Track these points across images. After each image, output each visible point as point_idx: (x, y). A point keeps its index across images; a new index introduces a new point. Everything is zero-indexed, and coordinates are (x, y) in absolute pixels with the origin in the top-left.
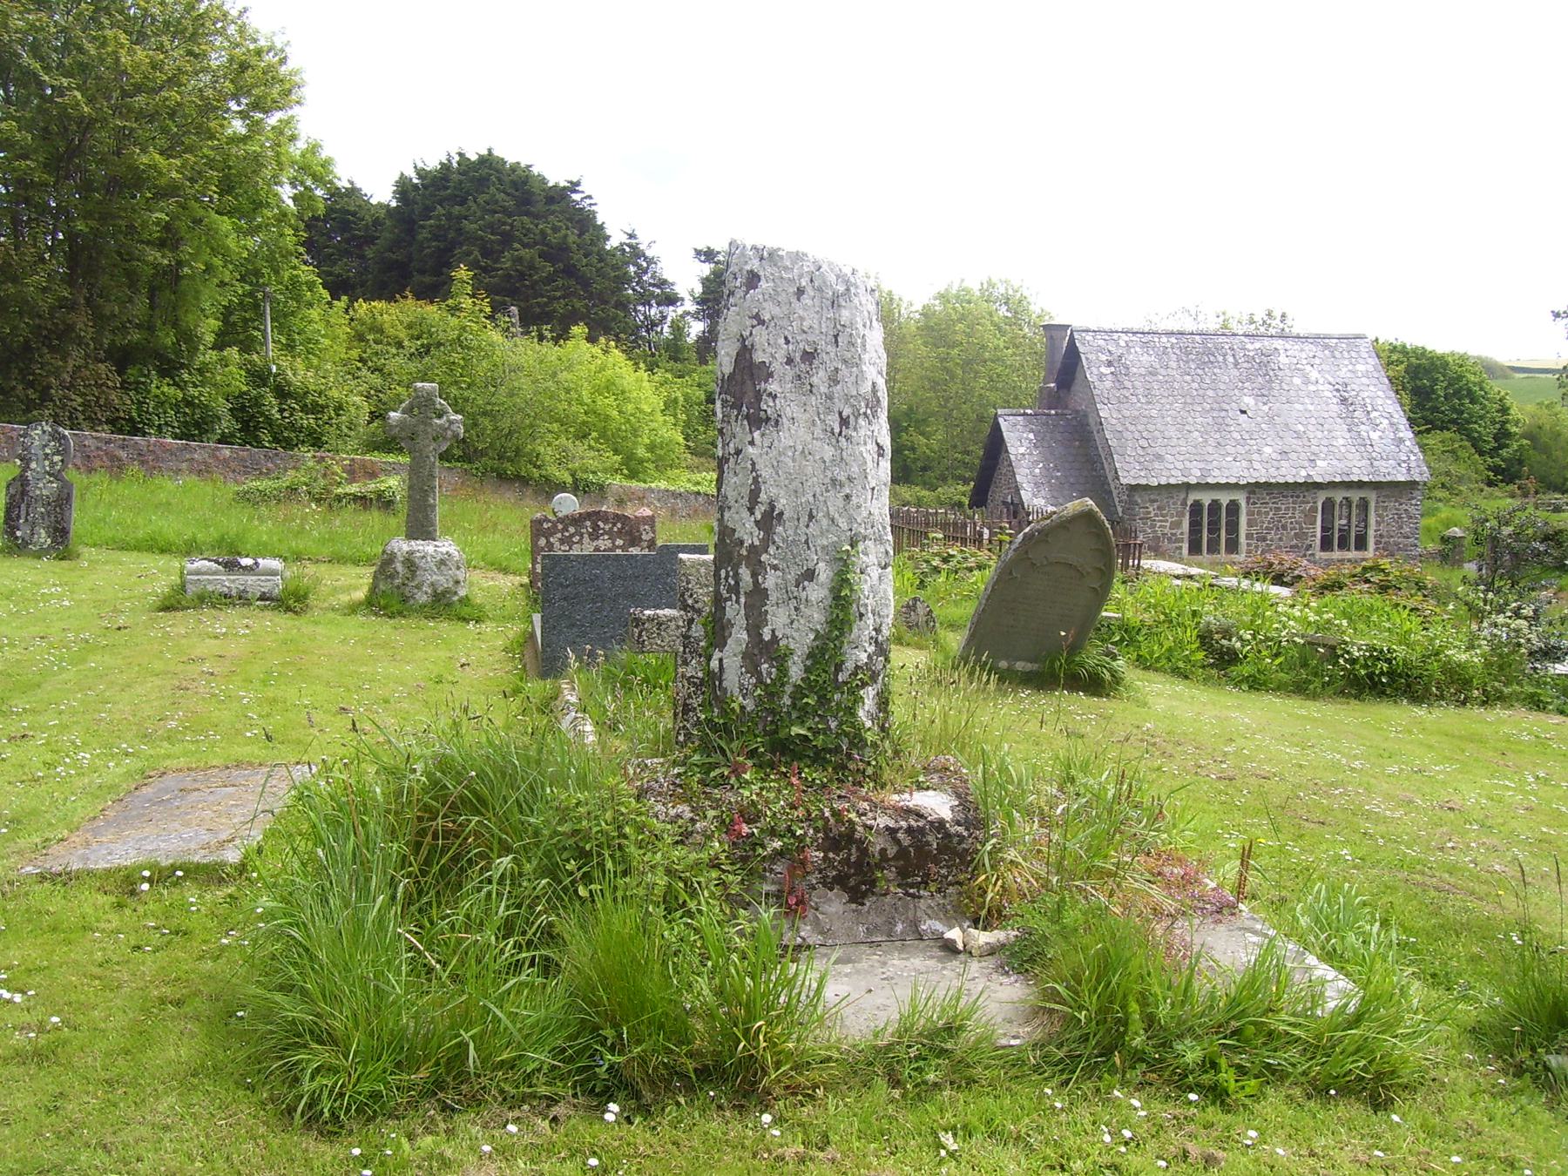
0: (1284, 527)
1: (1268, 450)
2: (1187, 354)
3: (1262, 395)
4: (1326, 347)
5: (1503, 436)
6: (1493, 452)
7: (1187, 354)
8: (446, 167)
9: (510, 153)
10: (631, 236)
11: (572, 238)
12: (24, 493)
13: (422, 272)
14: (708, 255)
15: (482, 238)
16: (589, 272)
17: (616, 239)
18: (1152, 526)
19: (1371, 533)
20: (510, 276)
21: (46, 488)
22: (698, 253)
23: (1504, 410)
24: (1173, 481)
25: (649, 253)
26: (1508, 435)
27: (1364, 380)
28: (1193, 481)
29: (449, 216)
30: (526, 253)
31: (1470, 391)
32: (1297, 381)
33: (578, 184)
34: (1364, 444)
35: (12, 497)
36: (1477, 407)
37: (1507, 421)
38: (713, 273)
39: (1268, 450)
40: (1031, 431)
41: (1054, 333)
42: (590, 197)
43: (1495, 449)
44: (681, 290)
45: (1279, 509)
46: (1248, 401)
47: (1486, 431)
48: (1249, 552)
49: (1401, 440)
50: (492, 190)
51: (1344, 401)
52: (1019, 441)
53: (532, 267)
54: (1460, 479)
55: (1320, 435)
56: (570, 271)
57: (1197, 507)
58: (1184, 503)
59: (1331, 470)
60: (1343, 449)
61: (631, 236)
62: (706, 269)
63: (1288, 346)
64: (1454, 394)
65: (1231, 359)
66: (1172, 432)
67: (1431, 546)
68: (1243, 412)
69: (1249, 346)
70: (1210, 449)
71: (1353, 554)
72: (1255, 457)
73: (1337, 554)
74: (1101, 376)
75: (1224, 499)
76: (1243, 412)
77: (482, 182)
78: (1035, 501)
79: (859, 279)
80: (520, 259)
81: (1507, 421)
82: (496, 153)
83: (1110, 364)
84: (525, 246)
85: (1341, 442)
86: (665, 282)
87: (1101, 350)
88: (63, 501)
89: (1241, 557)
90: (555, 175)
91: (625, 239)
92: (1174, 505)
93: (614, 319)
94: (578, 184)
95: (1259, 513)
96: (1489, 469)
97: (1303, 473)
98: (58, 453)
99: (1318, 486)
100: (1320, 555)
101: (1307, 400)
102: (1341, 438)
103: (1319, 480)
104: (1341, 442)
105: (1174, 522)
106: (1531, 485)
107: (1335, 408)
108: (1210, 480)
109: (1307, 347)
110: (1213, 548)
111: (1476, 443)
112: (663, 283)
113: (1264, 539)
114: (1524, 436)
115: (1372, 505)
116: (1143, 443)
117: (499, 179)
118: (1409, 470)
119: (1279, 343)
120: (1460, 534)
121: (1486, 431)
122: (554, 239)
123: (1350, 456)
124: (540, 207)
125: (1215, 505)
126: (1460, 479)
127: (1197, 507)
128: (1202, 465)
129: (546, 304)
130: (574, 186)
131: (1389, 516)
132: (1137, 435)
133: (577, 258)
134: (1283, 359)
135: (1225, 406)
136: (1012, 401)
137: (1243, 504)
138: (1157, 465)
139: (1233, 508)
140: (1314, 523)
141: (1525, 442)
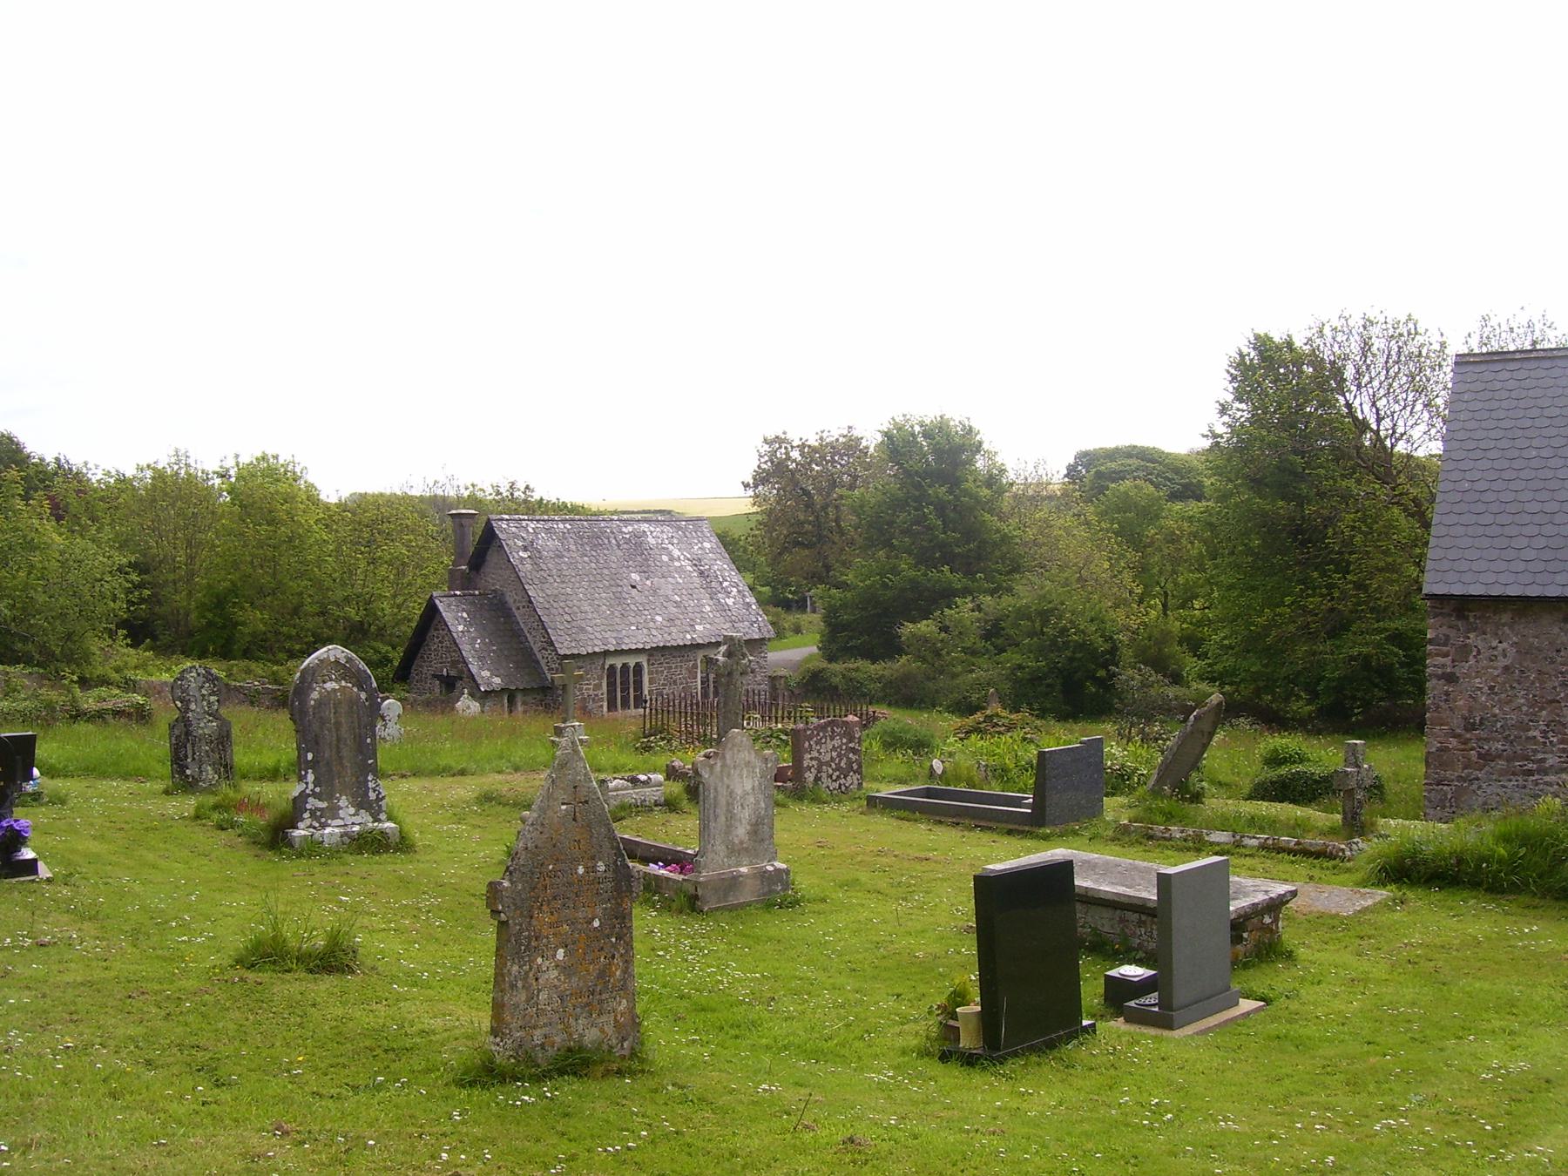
1: (659, 618)
3: (645, 572)
4: (679, 528)
12: (188, 733)
21: (207, 727)
24: (597, 650)
28: (612, 649)
32: (665, 558)
34: (724, 609)
35: (177, 737)
39: (659, 618)
41: (464, 521)
49: (749, 605)
52: (456, 618)
57: (612, 667)
83: (525, 549)
87: (516, 536)
88: (223, 740)
98: (213, 693)
99: (699, 646)
105: (595, 686)
108: (624, 647)
116: (567, 617)
127: (612, 667)
134: (651, 540)
137: (645, 665)
138: (582, 636)
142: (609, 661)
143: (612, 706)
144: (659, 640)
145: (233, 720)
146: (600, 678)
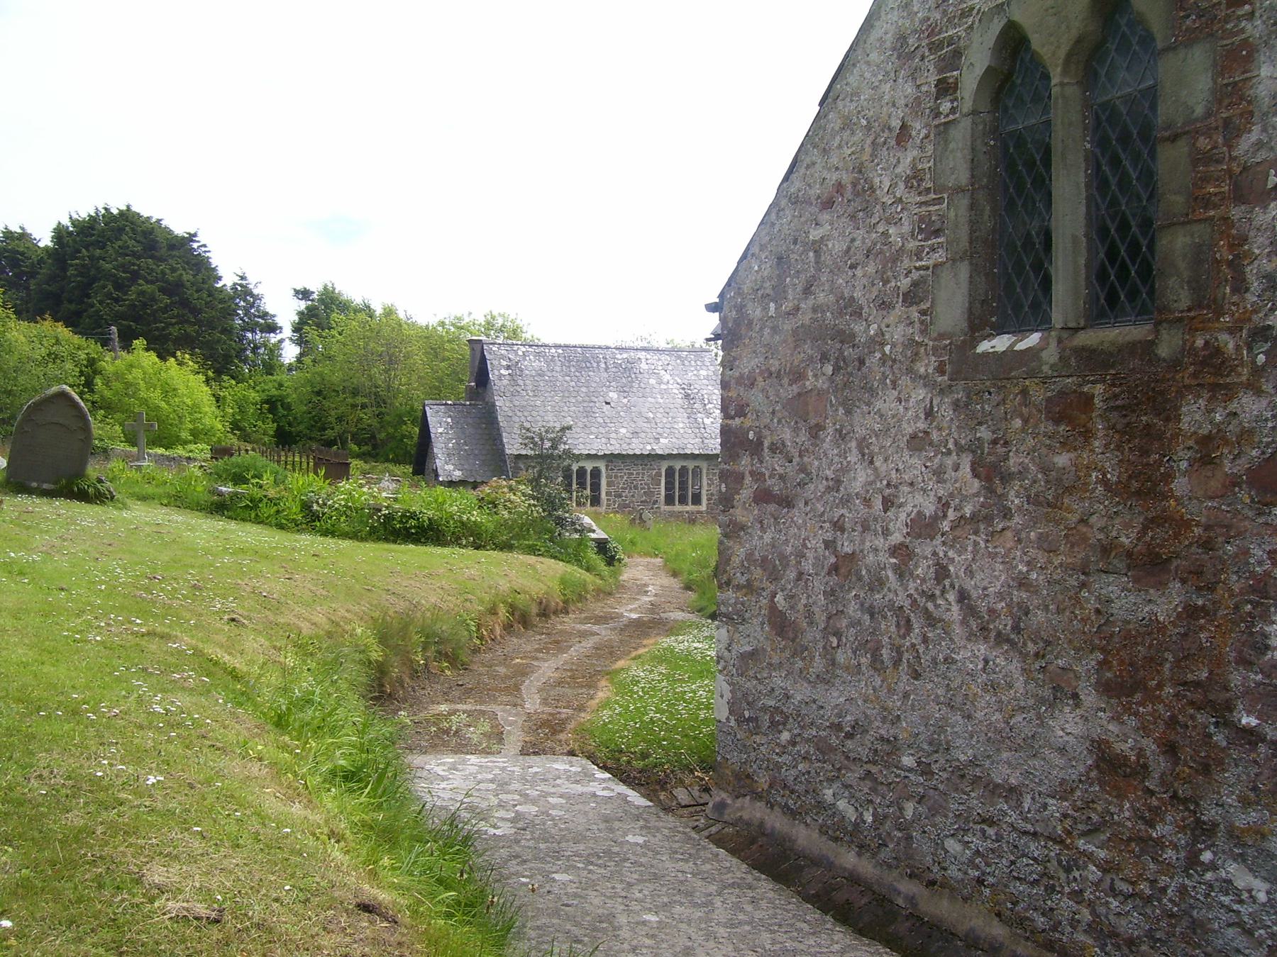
0: (636, 488)
1: (623, 431)
2: (569, 361)
3: (623, 391)
4: (679, 357)
7: (569, 361)
8: (93, 220)
9: (147, 208)
10: (242, 278)
11: (185, 277)
13: (70, 302)
14: (304, 294)
15: (115, 275)
16: (199, 304)
17: (228, 279)
19: (704, 492)
20: (135, 306)
22: (297, 292)
25: (256, 292)
27: (705, 382)
29: (91, 258)
30: (148, 288)
33: (195, 235)
38: (307, 308)
42: (205, 246)
44: (280, 321)
46: (613, 395)
48: (608, 505)
50: (125, 237)
51: (687, 396)
53: (153, 299)
56: (185, 303)
61: (242, 278)
62: (302, 305)
69: (618, 356)
71: (690, 508)
72: (613, 435)
73: (678, 508)
74: (500, 377)
77: (121, 230)
78: (446, 467)
79: (495, 313)
80: (142, 293)
82: (134, 209)
83: (508, 367)
84: (147, 282)
85: (681, 425)
86: (266, 314)
87: (503, 357)
90: (179, 227)
91: (237, 280)
93: (218, 341)
94: (195, 235)
95: (616, 477)
97: (649, 447)
99: (661, 457)
104: (681, 425)
109: (663, 357)
112: (265, 315)
113: (620, 496)
115: (704, 471)
117: (133, 230)
119: (642, 355)
122: (171, 277)
124: (163, 252)
129: (164, 329)
130: (192, 237)
132: (523, 419)
133: (190, 292)
134: (644, 366)
136: (437, 393)
137: (603, 470)
139: (596, 473)
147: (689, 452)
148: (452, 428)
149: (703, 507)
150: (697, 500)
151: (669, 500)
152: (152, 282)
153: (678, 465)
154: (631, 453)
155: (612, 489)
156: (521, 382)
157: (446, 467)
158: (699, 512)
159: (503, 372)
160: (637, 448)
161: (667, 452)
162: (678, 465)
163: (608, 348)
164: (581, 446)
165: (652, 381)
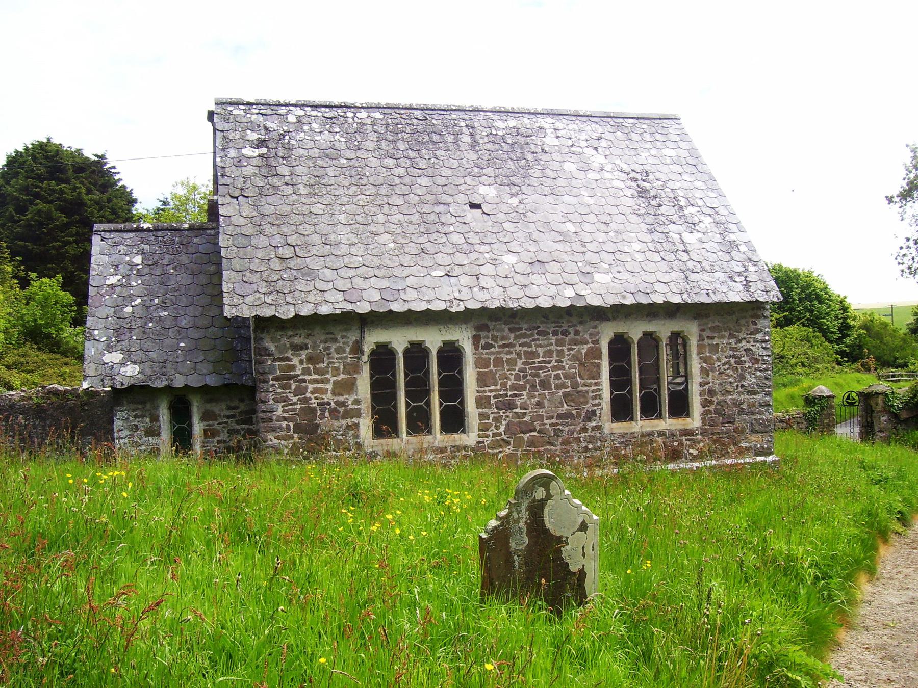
0: (545, 384)
1: (511, 259)
3: (508, 183)
5: (845, 328)
6: (839, 341)
18: (300, 391)
23: (845, 309)
24: (325, 310)
26: (849, 327)
28: (363, 308)
31: (817, 295)
36: (824, 307)
37: (847, 317)
40: (142, 252)
42: (114, 167)
43: (840, 339)
45: (534, 354)
46: (487, 192)
47: (833, 325)
48: (484, 428)
51: (642, 193)
53: (51, 219)
54: (816, 360)
55: (601, 237)
58: (357, 349)
59: (618, 288)
60: (639, 257)
63: (559, 125)
64: (806, 298)
65: (466, 139)
66: (343, 235)
67: (794, 411)
68: (474, 206)
70: (406, 260)
71: (668, 424)
72: (488, 269)
73: (640, 425)
75: (433, 339)
76: (474, 206)
80: (39, 212)
81: (847, 317)
83: (261, 143)
85: (637, 246)
87: (252, 126)
89: (470, 438)
91: (159, 205)
92: (338, 354)
96: (837, 353)
97: (570, 292)
99: (598, 314)
100: (611, 427)
101: (583, 192)
102: (636, 239)
103: (595, 302)
104: (637, 246)
106: (872, 363)
107: (629, 202)
108: (397, 307)
110: (419, 422)
111: (825, 332)
113: (510, 406)
114: (860, 328)
115: (693, 343)
116: (287, 252)
118: (747, 285)
119: (546, 122)
120: (826, 393)
121: (833, 325)
123: (650, 267)
125: (417, 353)
126: (816, 360)
128: (385, 284)
129: (61, 247)
131: (721, 359)
135: (445, 198)
137: (467, 347)
139: (451, 357)
140: (597, 375)
141: (862, 331)
142: (373, 339)
143: (385, 424)
144: (492, 297)
145: (472, 541)
146: (355, 368)
147: (659, 299)
148: (139, 274)
149: (695, 421)
150: (680, 406)
151: (622, 410)
152: (51, 202)
153: (636, 331)
154: (529, 304)
155: (490, 391)
156: (284, 170)
157: (107, 358)
158: (687, 433)
159: (248, 151)
160: (545, 293)
161: (611, 300)
162: (636, 331)
163: (477, 110)
164: (411, 295)
165: (569, 167)
